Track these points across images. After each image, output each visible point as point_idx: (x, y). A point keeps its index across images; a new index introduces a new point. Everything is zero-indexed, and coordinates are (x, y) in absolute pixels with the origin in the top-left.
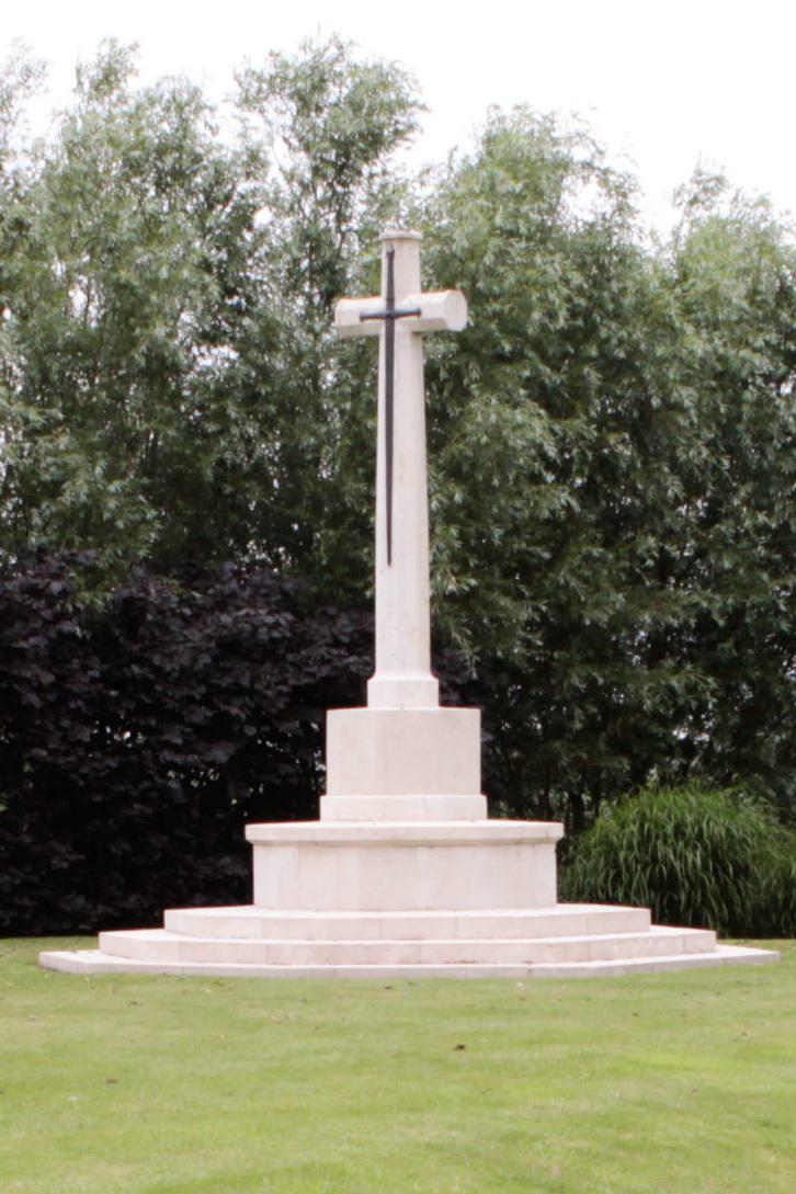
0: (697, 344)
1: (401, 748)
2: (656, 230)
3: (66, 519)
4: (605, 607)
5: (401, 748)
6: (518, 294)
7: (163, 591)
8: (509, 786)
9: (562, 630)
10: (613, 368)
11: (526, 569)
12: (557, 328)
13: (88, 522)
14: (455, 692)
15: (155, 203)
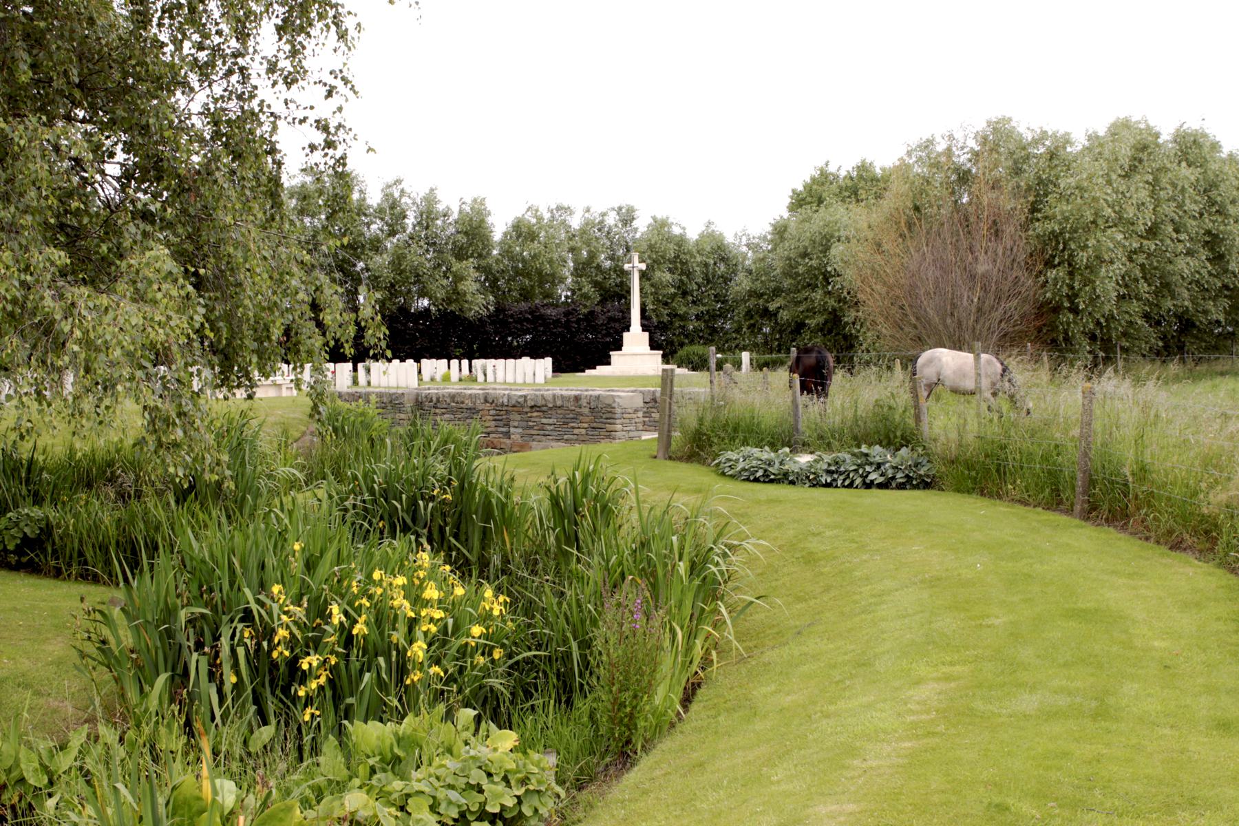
0: (699, 259)
1: (636, 338)
2: (693, 235)
3: (582, 295)
4: (682, 310)
5: (636, 338)
6: (665, 251)
7: (598, 309)
8: (654, 345)
9: (674, 315)
10: (682, 263)
11: (666, 304)
12: (668, 254)
13: (586, 296)
14: (645, 328)
15: (350, 507)
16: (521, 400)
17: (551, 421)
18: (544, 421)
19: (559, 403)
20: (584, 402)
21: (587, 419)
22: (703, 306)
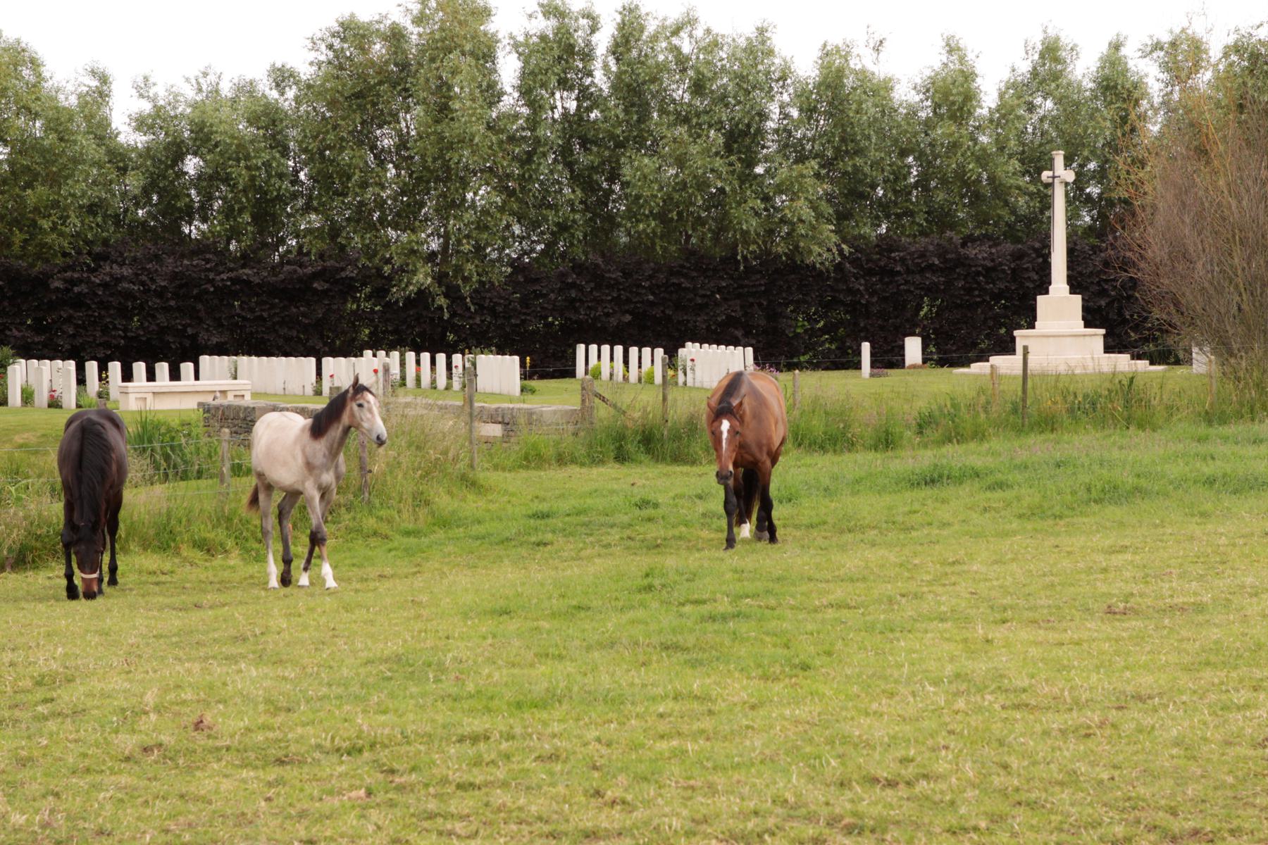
1: (1059, 307)
5: (1059, 307)
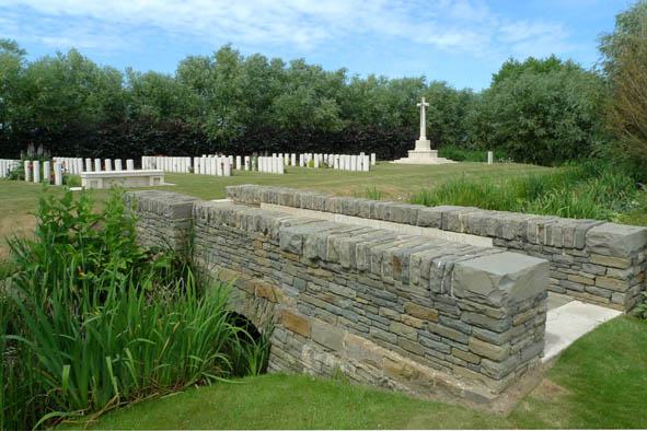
1: (422, 143)
5: (422, 143)
14: (428, 137)
16: (297, 243)
17: (346, 291)
18: (333, 287)
19: (361, 263)
20: (415, 274)
21: (425, 312)
22: (457, 127)
